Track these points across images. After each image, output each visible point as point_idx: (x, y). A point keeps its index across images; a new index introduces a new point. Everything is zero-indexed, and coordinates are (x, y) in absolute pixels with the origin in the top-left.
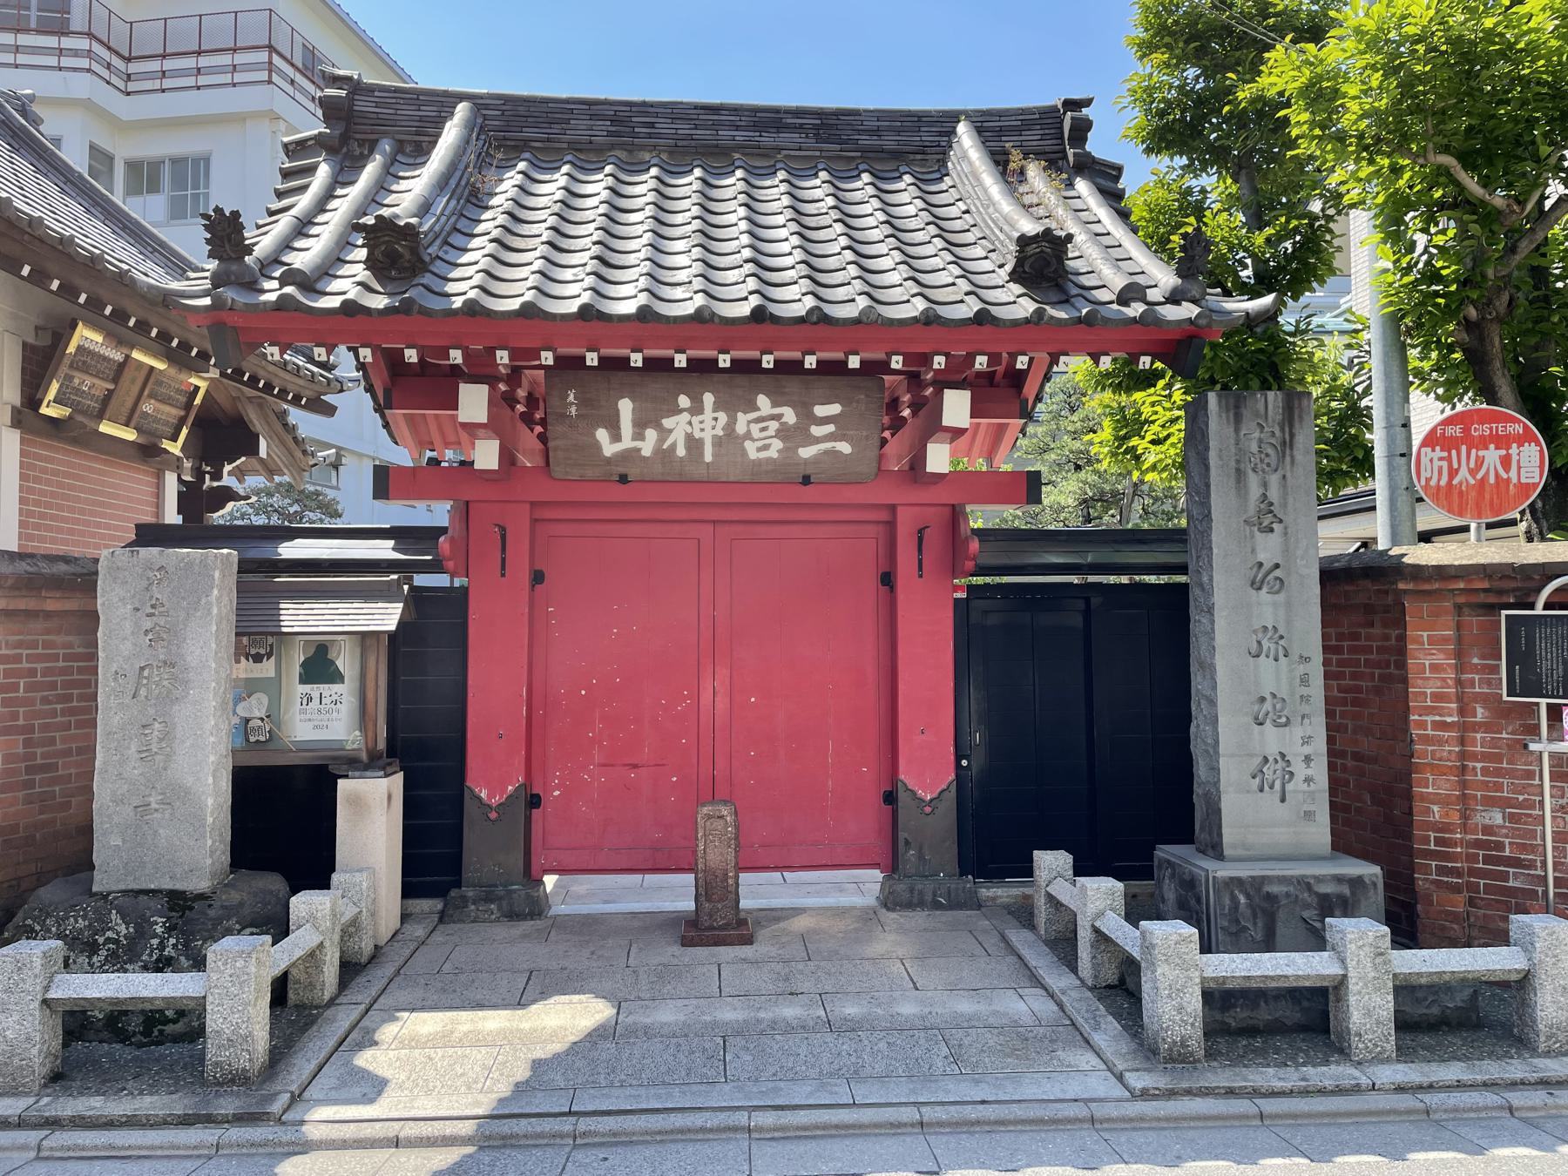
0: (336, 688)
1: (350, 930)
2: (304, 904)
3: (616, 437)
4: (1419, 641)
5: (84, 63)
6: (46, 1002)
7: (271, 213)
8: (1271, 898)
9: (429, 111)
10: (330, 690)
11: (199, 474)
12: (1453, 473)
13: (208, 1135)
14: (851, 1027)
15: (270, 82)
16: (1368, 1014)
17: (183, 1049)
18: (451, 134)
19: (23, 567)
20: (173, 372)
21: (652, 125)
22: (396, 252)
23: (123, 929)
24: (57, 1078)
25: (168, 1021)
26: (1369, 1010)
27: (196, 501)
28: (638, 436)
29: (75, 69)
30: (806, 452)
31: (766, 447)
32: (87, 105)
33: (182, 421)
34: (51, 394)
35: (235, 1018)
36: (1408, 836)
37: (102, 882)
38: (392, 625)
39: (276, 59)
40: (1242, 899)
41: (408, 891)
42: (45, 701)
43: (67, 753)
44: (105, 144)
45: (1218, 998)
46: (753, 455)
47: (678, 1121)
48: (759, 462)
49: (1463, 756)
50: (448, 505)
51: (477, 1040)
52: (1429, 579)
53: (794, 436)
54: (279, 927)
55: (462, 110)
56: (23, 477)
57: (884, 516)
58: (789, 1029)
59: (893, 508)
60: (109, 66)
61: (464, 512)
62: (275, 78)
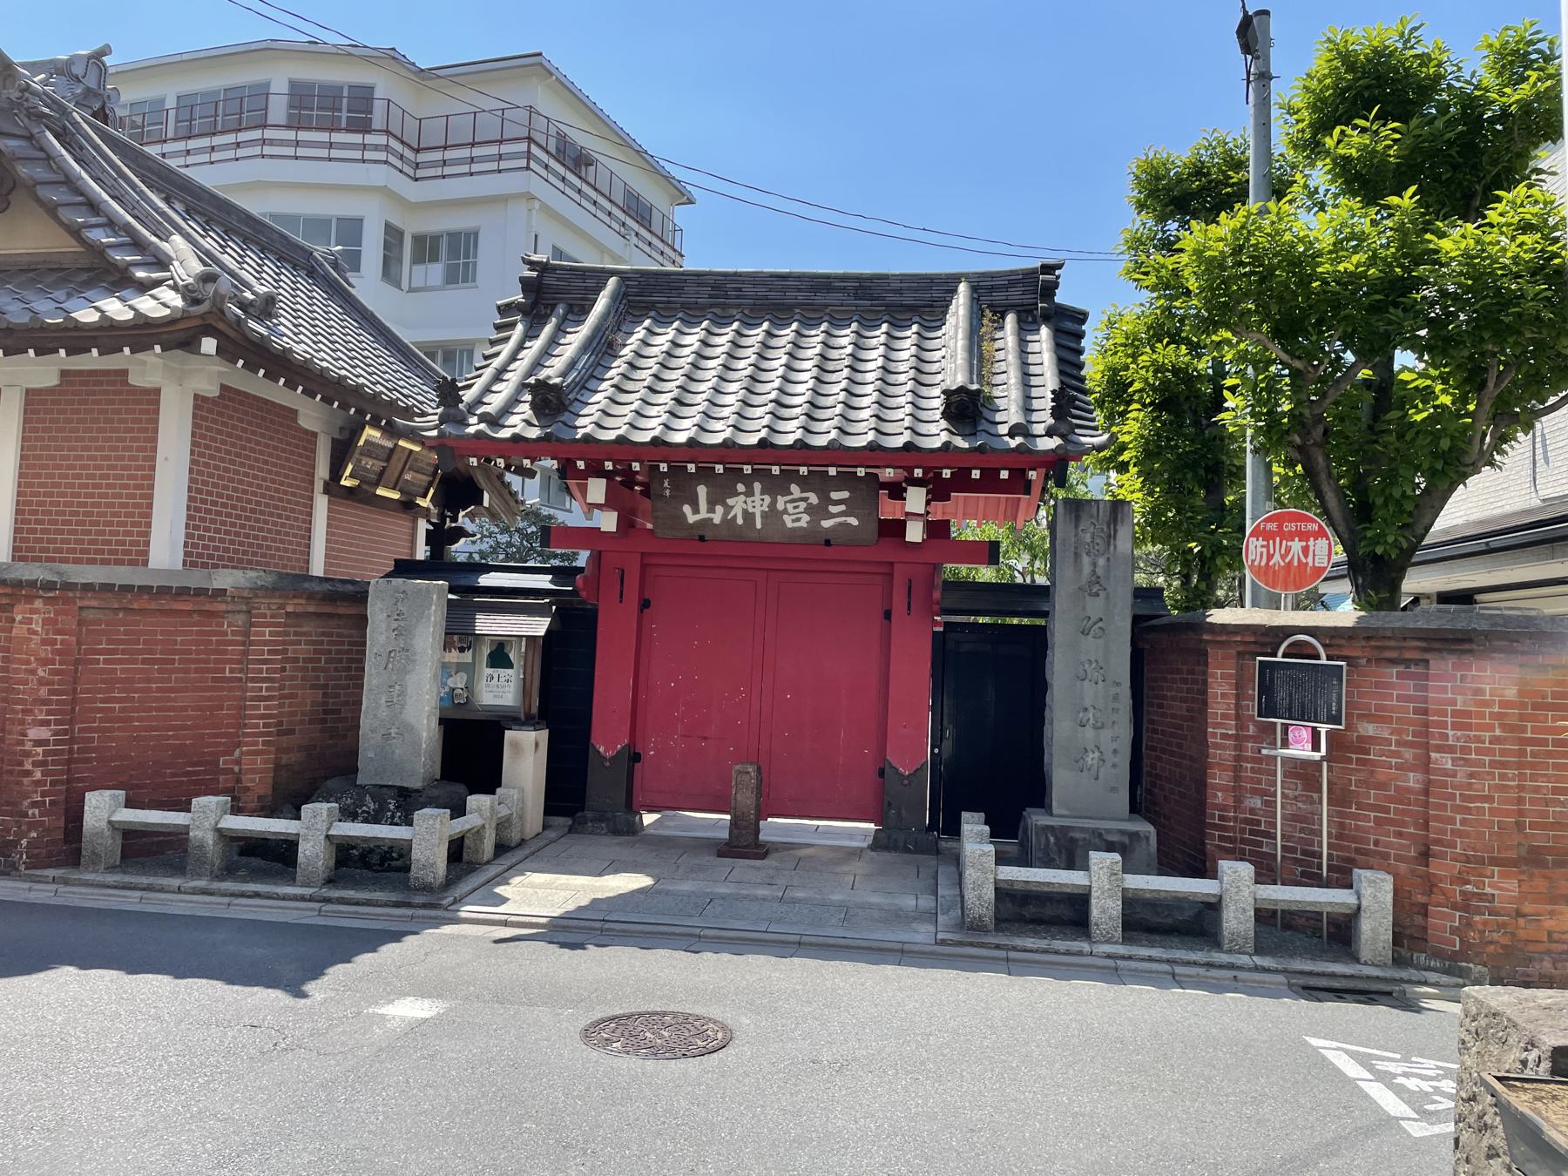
0: (510, 671)
1: (502, 825)
2: (473, 801)
3: (696, 511)
4: (1214, 676)
5: (382, 156)
6: (327, 837)
7: (486, 358)
8: (1073, 841)
9: (591, 283)
10: (505, 673)
11: (442, 517)
12: (1270, 557)
13: (409, 912)
14: (794, 901)
15: (528, 168)
16: (1104, 912)
17: (402, 875)
18: (601, 303)
19: (327, 586)
20: (425, 452)
21: (740, 290)
22: (551, 401)
23: (372, 806)
24: (330, 882)
25: (393, 859)
26: (1105, 909)
27: (441, 538)
28: (711, 510)
29: (375, 162)
30: (826, 524)
31: (798, 520)
32: (385, 191)
33: (430, 484)
34: (347, 473)
35: (427, 853)
36: (1203, 813)
37: (361, 779)
38: (541, 632)
39: (534, 149)
40: (1052, 839)
41: (550, 810)
42: (336, 669)
43: (346, 703)
44: (396, 222)
45: (1004, 893)
46: (789, 525)
47: (666, 929)
48: (794, 529)
49: (1238, 758)
50: (587, 553)
51: (566, 888)
52: (1220, 634)
53: (817, 512)
54: (459, 811)
55: (612, 282)
56: (329, 525)
57: (885, 569)
58: (756, 899)
59: (892, 564)
60: (402, 157)
61: (597, 558)
62: (533, 165)
